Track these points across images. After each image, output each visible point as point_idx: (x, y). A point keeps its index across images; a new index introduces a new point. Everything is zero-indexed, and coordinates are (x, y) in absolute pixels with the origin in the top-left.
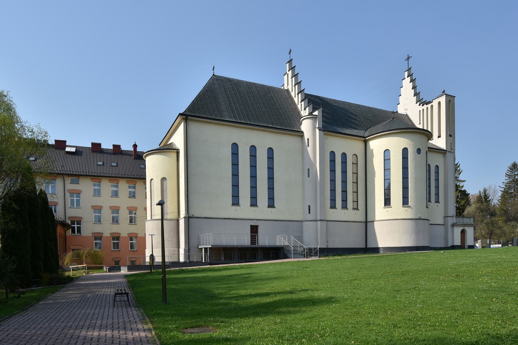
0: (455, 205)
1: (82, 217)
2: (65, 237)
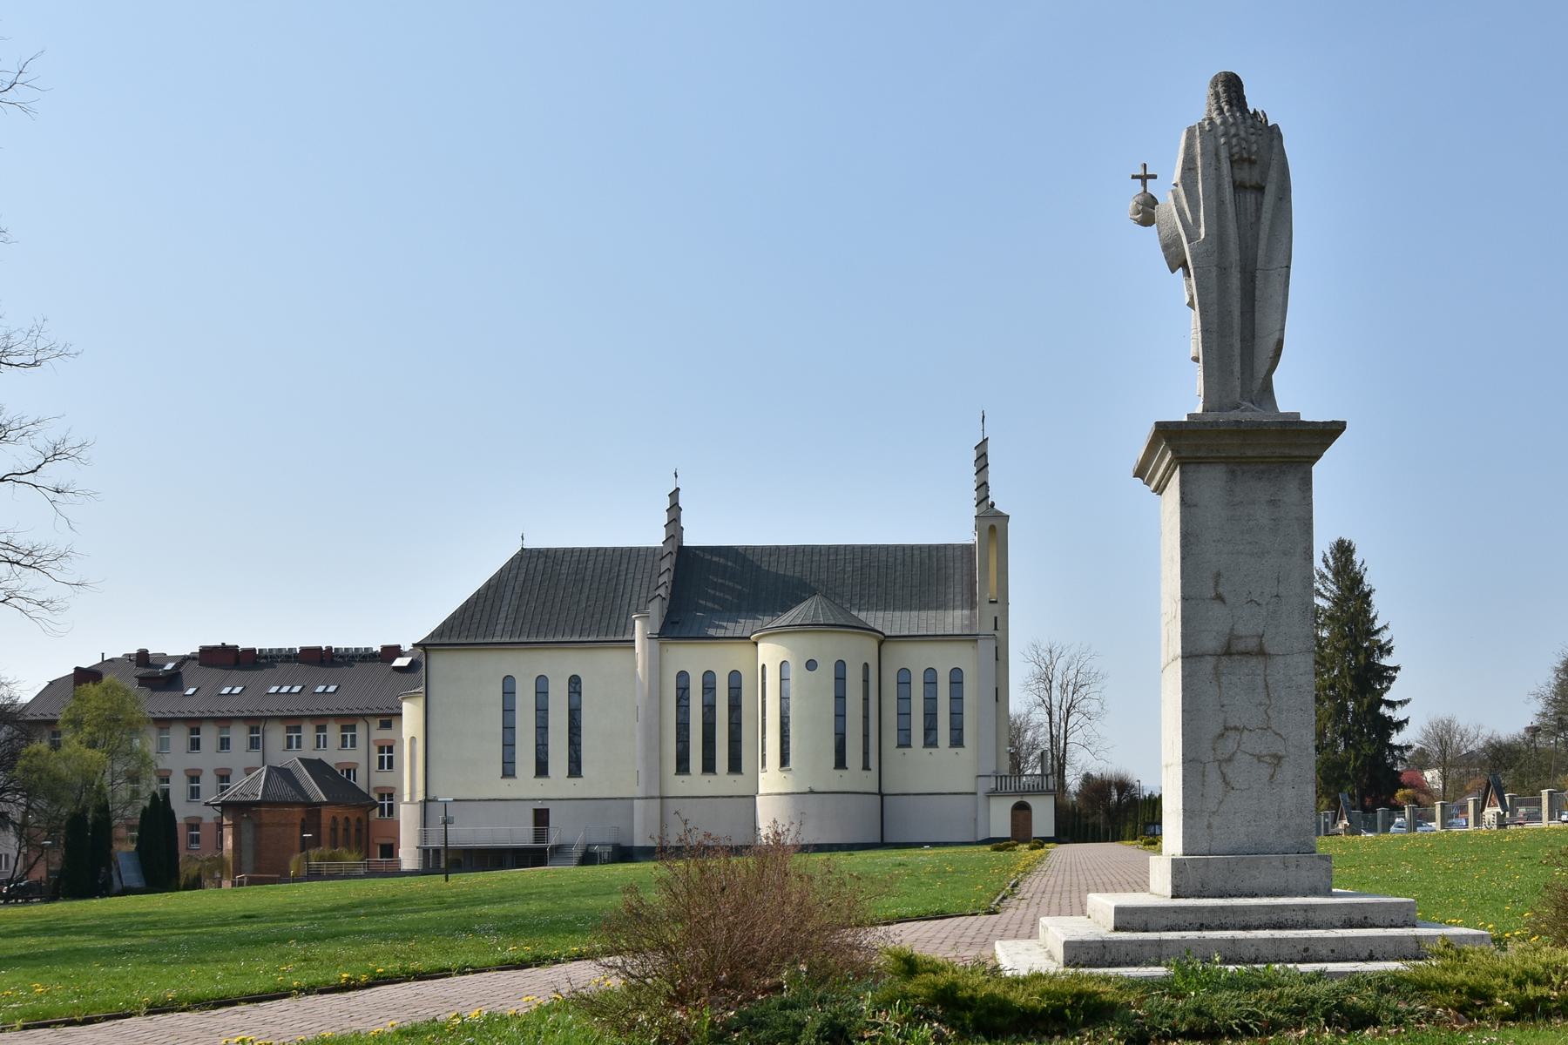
0: (1008, 748)
1: (392, 786)
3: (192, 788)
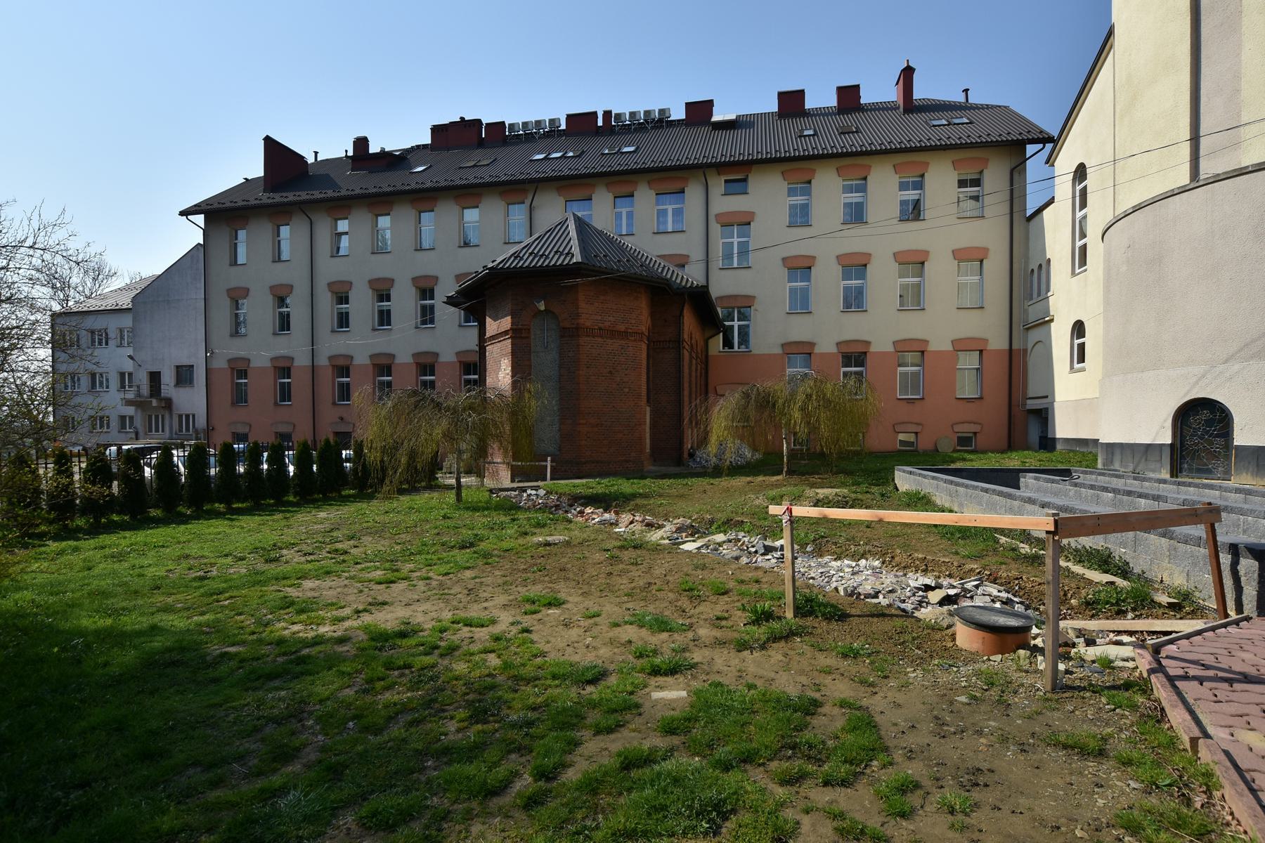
2: (706, 360)
3: (424, 308)
